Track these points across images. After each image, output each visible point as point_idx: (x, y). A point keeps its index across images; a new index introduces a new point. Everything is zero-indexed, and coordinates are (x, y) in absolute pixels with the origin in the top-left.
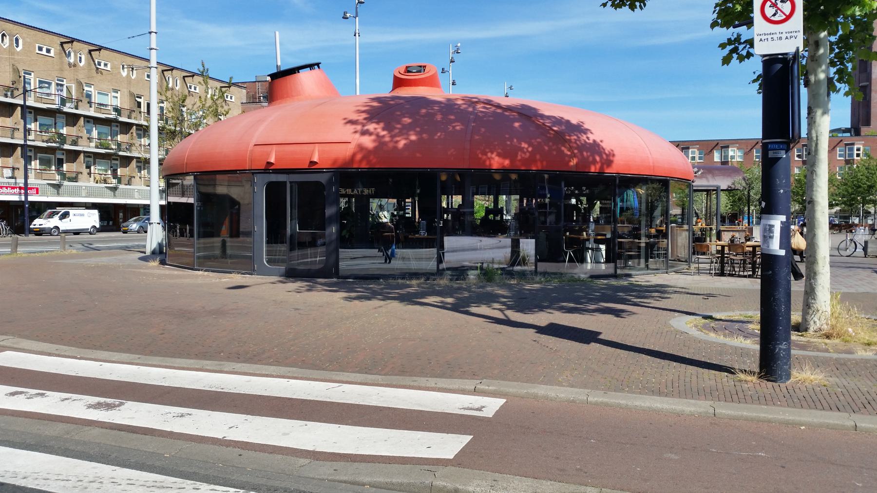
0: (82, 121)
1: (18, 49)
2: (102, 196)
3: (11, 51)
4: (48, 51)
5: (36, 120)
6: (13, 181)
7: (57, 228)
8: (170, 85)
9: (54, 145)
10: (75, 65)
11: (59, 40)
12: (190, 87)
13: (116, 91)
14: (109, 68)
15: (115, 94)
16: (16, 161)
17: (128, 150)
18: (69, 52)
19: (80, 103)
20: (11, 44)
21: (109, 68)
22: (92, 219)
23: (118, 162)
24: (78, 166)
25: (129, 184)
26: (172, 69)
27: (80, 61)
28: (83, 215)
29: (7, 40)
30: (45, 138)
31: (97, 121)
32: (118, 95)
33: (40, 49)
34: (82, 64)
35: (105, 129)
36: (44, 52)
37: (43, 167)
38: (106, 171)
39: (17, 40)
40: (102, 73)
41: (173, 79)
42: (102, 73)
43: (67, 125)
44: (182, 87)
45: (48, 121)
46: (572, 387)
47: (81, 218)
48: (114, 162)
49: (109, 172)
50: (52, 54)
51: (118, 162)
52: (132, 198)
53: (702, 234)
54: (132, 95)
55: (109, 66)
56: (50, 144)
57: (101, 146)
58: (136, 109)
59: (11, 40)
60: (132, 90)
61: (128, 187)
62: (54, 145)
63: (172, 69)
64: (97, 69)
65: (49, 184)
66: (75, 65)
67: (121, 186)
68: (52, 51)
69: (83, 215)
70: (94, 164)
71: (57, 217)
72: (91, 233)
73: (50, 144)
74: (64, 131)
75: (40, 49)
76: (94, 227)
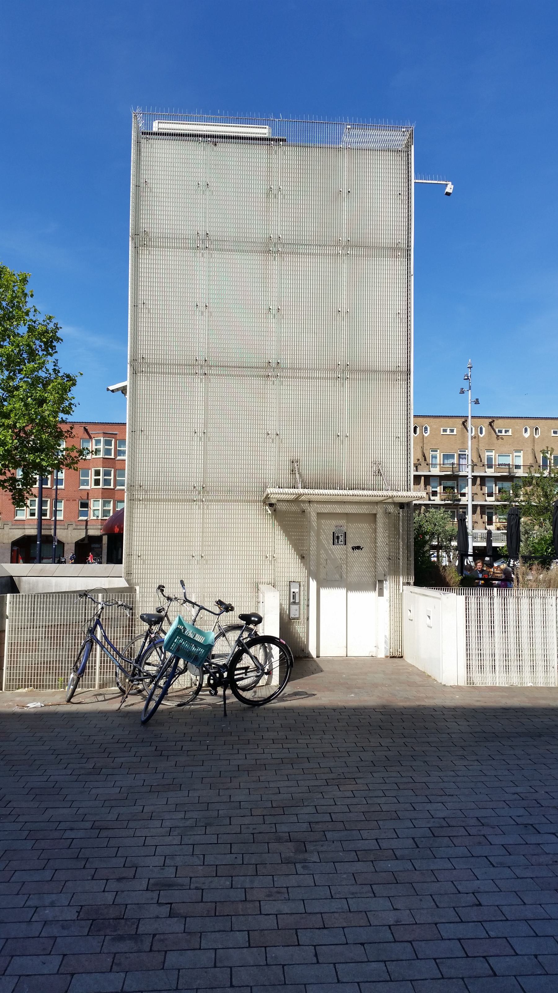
4: (452, 431)
5: (441, 485)
9: (449, 502)
12: (500, 431)
21: (510, 433)
27: (481, 433)
31: (497, 479)
32: (521, 454)
36: (448, 432)
39: (481, 429)
40: (502, 439)
42: (502, 439)
46: (415, 539)
50: (455, 433)
53: (29, 433)
56: (446, 502)
62: (449, 502)
64: (498, 436)
70: (496, 514)
73: (446, 502)
75: (445, 431)
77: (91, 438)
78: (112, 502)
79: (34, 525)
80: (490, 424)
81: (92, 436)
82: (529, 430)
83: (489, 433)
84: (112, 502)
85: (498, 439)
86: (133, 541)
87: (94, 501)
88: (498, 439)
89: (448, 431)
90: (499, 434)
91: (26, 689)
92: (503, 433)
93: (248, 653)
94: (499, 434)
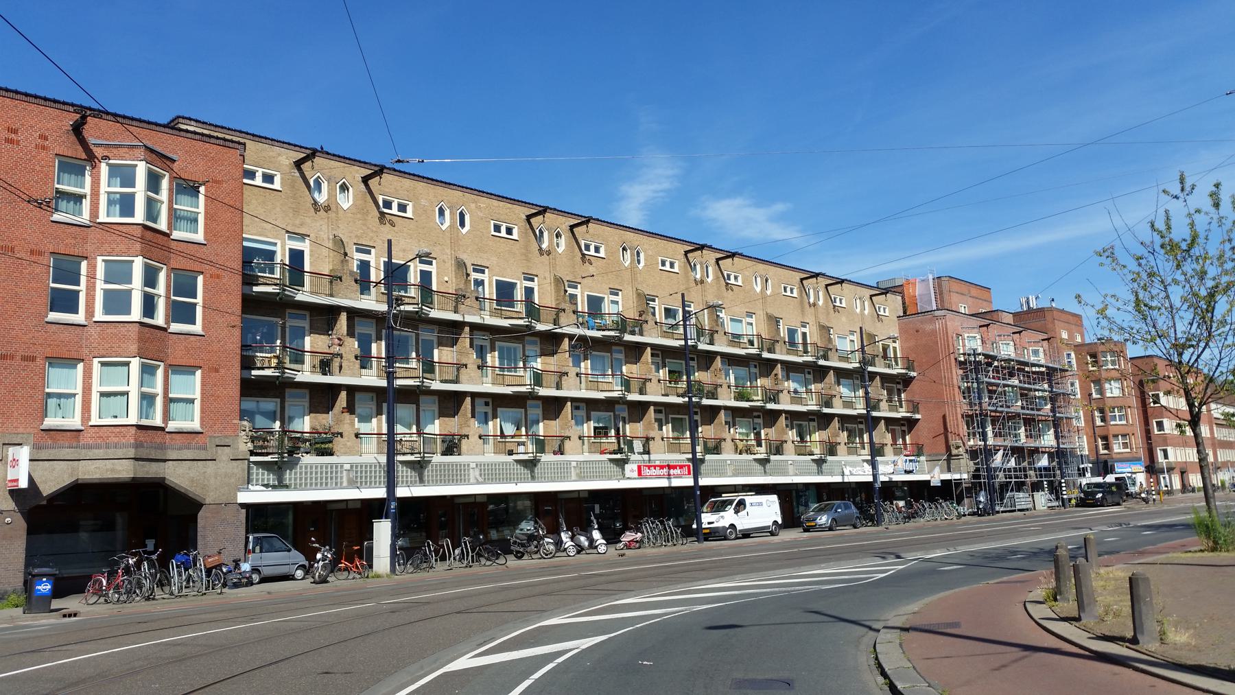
0: (718, 362)
1: (464, 231)
2: (508, 480)
3: (633, 268)
4: (672, 265)
6: (646, 457)
7: (732, 526)
8: (812, 301)
10: (702, 282)
11: (524, 212)
12: (388, 204)
13: (750, 314)
14: (602, 254)
15: (749, 320)
16: (648, 427)
17: (713, 395)
18: (541, 232)
19: (562, 314)
20: (632, 261)
22: (765, 511)
23: (760, 421)
24: (464, 423)
25: (561, 451)
26: (702, 247)
27: (462, 224)
28: (760, 504)
29: (628, 254)
30: (680, 391)
33: (497, 228)
34: (709, 280)
35: (743, 371)
37: (676, 434)
38: (747, 435)
39: (462, 216)
40: (393, 225)
41: (701, 264)
43: (543, 354)
44: (825, 300)
45: (679, 364)
47: (760, 508)
48: (756, 420)
49: (752, 436)
50: (277, 185)
51: (760, 421)
52: (785, 474)
54: (558, 281)
55: (602, 250)
57: (740, 397)
58: (566, 306)
59: (632, 255)
60: (464, 257)
61: (559, 457)
63: (702, 247)
65: (611, 460)
66: (702, 282)
67: (546, 458)
68: (515, 231)
69: (760, 504)
71: (730, 510)
72: (772, 534)
74: (698, 376)
75: (663, 264)
76: (775, 522)
77: (91, 158)
78: (160, 373)
79: (125, 446)
80: (77, 129)
81: (99, 152)
82: (325, 186)
83: (717, 278)
84: (160, 373)
85: (584, 262)
86: (1106, 245)
87: (103, 364)
88: (584, 262)
89: (259, 176)
90: (386, 211)
91: (963, 406)
92: (394, 210)
93: (985, 445)
94: (386, 211)
